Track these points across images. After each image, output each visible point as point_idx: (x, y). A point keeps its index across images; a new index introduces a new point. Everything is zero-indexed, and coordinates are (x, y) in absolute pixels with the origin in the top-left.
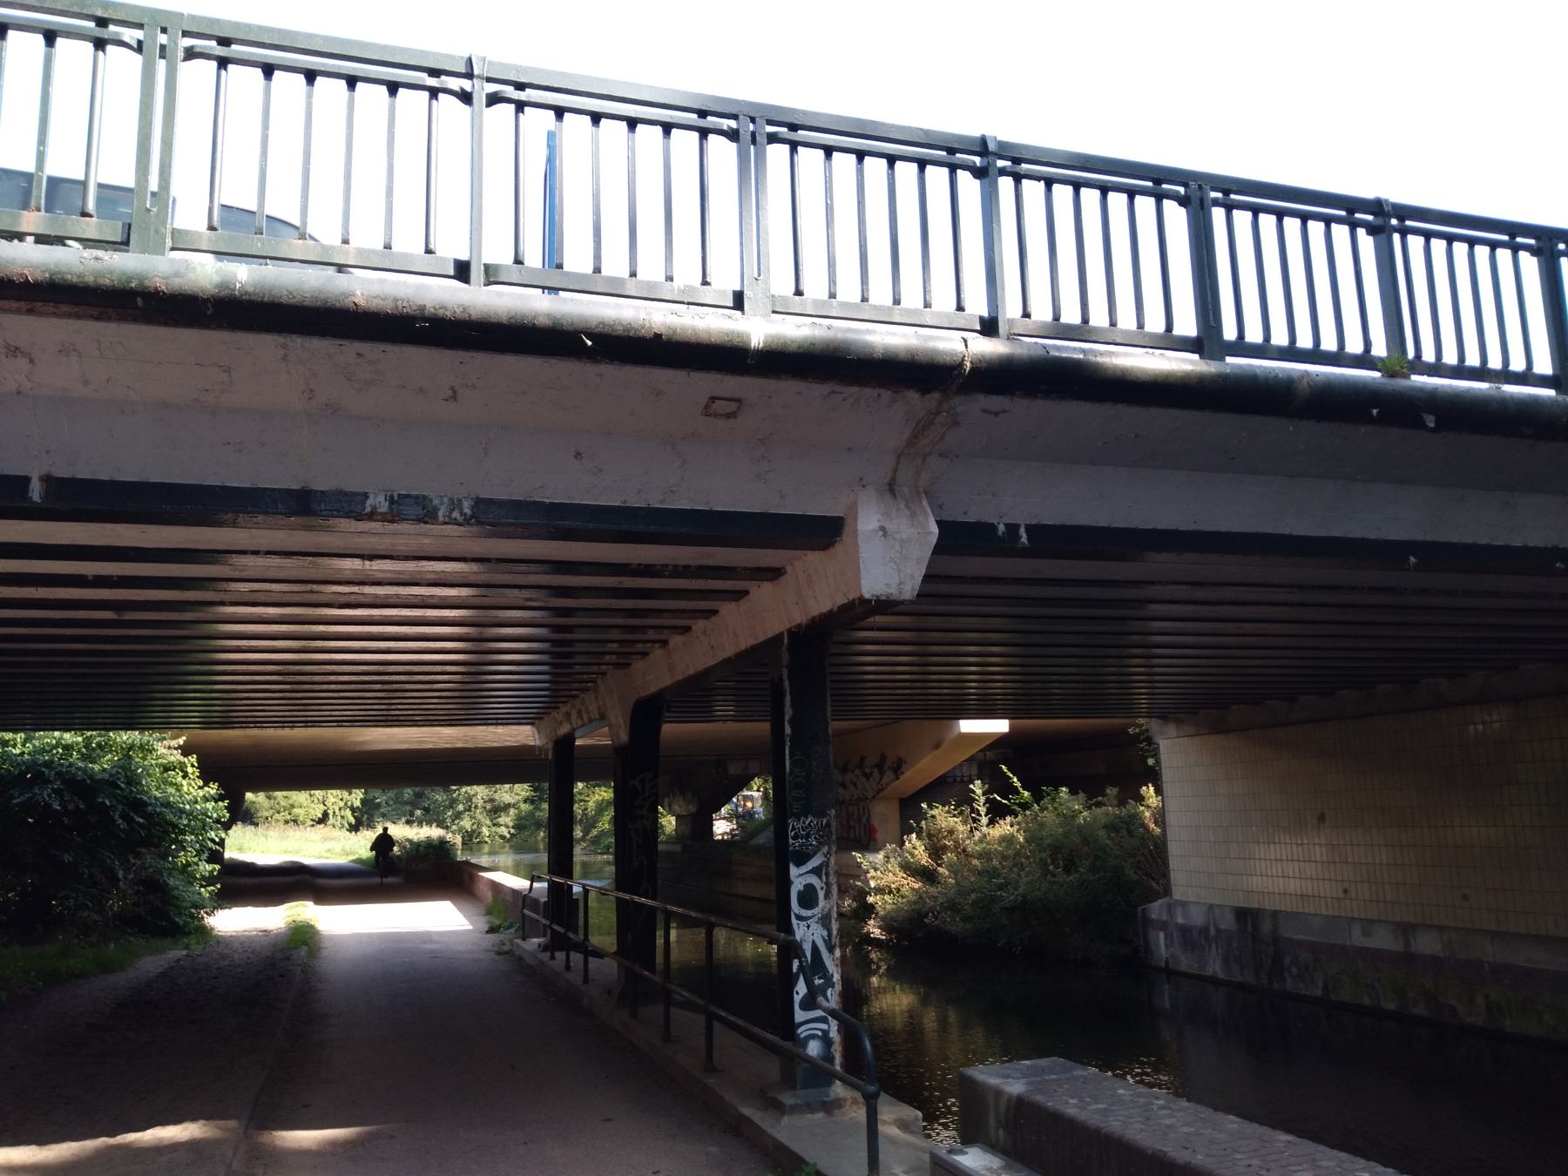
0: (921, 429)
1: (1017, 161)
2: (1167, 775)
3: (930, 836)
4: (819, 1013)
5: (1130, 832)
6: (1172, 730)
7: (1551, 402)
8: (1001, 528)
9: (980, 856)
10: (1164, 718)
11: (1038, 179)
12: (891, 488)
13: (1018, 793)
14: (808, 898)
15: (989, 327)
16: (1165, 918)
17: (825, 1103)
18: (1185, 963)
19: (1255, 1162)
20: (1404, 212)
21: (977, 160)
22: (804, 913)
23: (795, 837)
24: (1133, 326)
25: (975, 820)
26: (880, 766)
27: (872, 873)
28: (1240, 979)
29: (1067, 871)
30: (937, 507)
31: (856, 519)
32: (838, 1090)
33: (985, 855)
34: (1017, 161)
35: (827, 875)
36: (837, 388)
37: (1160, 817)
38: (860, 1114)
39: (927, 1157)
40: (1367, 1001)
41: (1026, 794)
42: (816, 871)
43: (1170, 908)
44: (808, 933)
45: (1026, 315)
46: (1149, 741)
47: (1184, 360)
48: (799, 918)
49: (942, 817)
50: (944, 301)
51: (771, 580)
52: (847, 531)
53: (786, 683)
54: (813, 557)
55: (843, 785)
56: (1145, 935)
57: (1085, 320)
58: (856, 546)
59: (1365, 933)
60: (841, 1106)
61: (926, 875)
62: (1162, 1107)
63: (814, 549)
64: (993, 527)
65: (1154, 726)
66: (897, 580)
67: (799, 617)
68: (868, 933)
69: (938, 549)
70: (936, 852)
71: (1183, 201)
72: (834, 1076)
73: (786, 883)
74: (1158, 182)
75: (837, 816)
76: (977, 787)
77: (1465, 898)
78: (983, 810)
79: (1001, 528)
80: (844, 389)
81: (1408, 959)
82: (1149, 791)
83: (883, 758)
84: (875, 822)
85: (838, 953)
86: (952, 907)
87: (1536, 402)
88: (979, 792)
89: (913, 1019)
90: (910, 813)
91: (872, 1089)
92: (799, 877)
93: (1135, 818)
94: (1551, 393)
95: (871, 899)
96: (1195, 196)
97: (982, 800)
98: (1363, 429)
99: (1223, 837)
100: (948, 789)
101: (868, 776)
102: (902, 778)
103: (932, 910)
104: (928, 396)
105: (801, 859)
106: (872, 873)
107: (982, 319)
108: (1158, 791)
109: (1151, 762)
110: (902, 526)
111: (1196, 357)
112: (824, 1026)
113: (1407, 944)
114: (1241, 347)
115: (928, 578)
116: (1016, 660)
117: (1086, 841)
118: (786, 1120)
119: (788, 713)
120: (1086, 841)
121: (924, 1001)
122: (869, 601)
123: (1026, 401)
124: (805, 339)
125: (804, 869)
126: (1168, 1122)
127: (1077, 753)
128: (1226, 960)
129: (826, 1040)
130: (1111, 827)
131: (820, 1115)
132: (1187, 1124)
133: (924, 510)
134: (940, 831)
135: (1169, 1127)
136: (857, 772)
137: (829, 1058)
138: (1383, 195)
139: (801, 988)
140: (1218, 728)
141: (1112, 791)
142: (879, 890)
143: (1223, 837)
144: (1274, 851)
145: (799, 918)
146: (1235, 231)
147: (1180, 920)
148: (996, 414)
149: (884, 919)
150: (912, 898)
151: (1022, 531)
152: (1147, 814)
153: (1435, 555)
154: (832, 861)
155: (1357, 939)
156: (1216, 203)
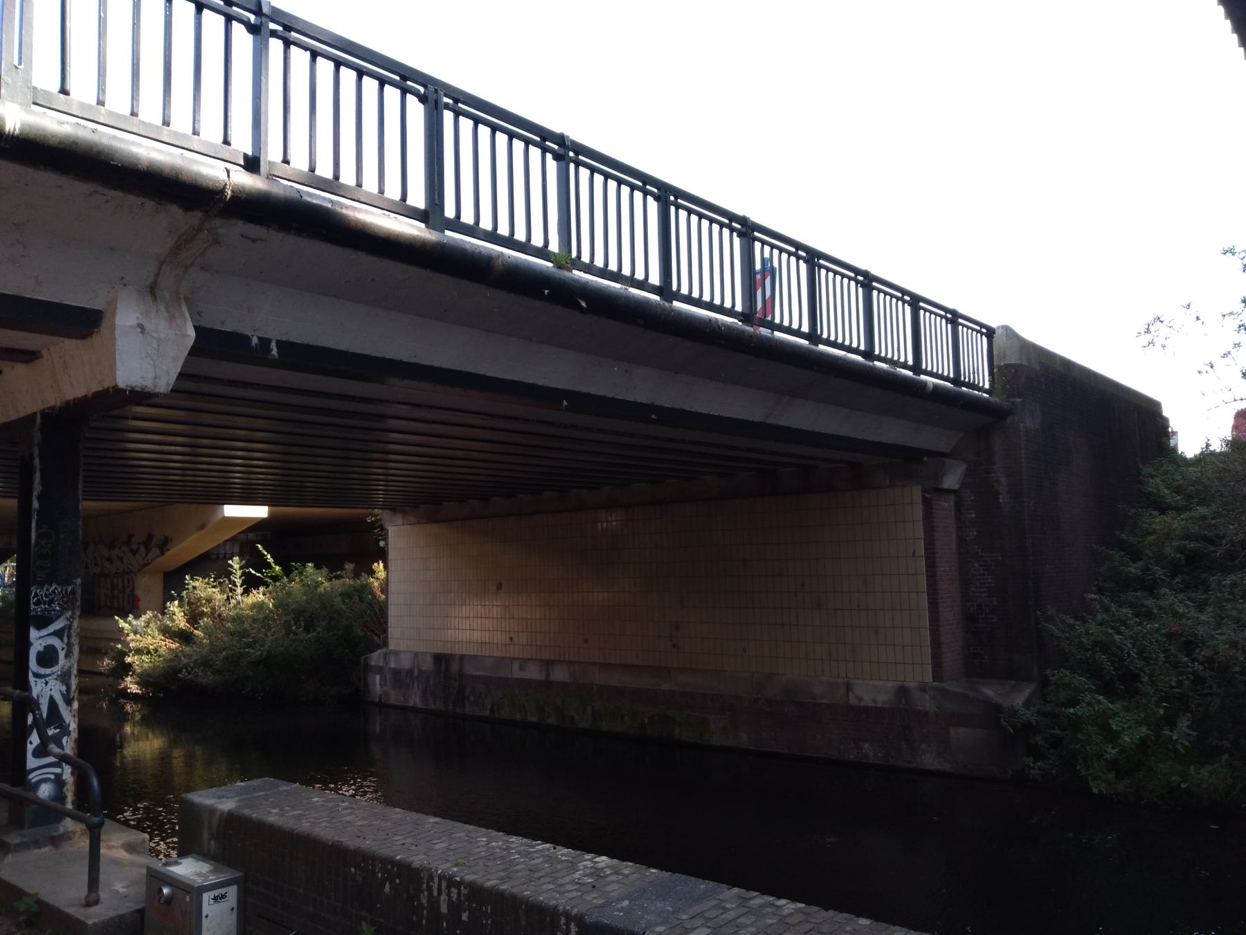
0: (183, 242)
1: (288, 28)
2: (392, 554)
3: (189, 603)
4: (51, 759)
5: (361, 598)
6: (399, 519)
7: (657, 305)
8: (255, 341)
9: (234, 620)
10: (393, 510)
11: (306, 49)
12: (153, 291)
13: (271, 567)
14: (48, 658)
15: (252, 164)
16: (381, 664)
17: (53, 838)
18: (394, 698)
19: (410, 840)
20: (580, 149)
21: (252, 18)
22: (43, 671)
23: (38, 603)
24: (375, 191)
25: (231, 590)
26: (147, 544)
27: (132, 636)
28: (433, 707)
29: (307, 630)
30: (195, 313)
31: (114, 314)
32: (69, 824)
33: (238, 619)
34: (288, 28)
35: (69, 637)
36: (100, 189)
37: (385, 588)
38: (84, 844)
39: (144, 871)
40: (518, 717)
41: (278, 568)
42: (58, 634)
43: (386, 656)
44: (45, 688)
45: (286, 161)
46: (382, 528)
47: (413, 226)
48: (36, 675)
49: (200, 587)
50: (212, 132)
51: (27, 362)
52: (105, 324)
53: (37, 461)
54: (70, 344)
55: (110, 560)
56: (366, 679)
57: (337, 177)
58: (113, 339)
59: (521, 668)
60: (70, 839)
61: (184, 637)
62: (346, 808)
63: (70, 337)
64: (247, 339)
65: (385, 515)
66: (151, 375)
67: (52, 399)
68: (126, 688)
69: (194, 352)
70: (193, 618)
71: (423, 99)
72: (62, 814)
73: (25, 644)
74: (404, 78)
75: (83, 584)
76: (235, 563)
77: (586, 641)
78: (239, 582)
79: (255, 341)
80: (106, 191)
81: (548, 684)
82: (379, 567)
83: (150, 537)
84: (139, 593)
85: (76, 705)
86: (205, 663)
87: (647, 302)
88: (236, 566)
89: (164, 758)
90: (173, 582)
91: (96, 820)
92: (38, 640)
93: (367, 588)
94: (657, 298)
95: (128, 660)
96: (432, 97)
97: (239, 573)
98: (538, 304)
99: (430, 601)
100: (209, 564)
101: (134, 552)
102: (168, 554)
103: (186, 666)
104: (190, 213)
105: (42, 623)
106: (132, 636)
107: (246, 156)
108: (386, 567)
109: (382, 544)
110: (159, 325)
111: (423, 225)
112: (58, 770)
113: (548, 675)
114: (456, 224)
115: (181, 376)
116: (278, 456)
117: (324, 606)
118: (10, 858)
119: (37, 488)
120: (324, 606)
121: (173, 743)
122: (123, 391)
123: (281, 235)
124: (67, 136)
125: (44, 632)
126: (348, 818)
127: (320, 537)
128: (424, 693)
129: (59, 782)
130: (346, 595)
131: (47, 849)
132: (363, 819)
133: (184, 318)
134: (199, 599)
135: (348, 822)
136: (124, 548)
137: (60, 797)
138: (566, 133)
139: (35, 739)
140: (433, 519)
141: (349, 567)
142: (139, 651)
143: (430, 601)
144: (465, 611)
145: (36, 675)
146: (460, 133)
147: (393, 665)
148: (254, 241)
149: (140, 676)
150: (168, 656)
151: (273, 345)
152: (376, 584)
153: (581, 401)
154: (76, 624)
155: (517, 673)
156: (447, 107)
